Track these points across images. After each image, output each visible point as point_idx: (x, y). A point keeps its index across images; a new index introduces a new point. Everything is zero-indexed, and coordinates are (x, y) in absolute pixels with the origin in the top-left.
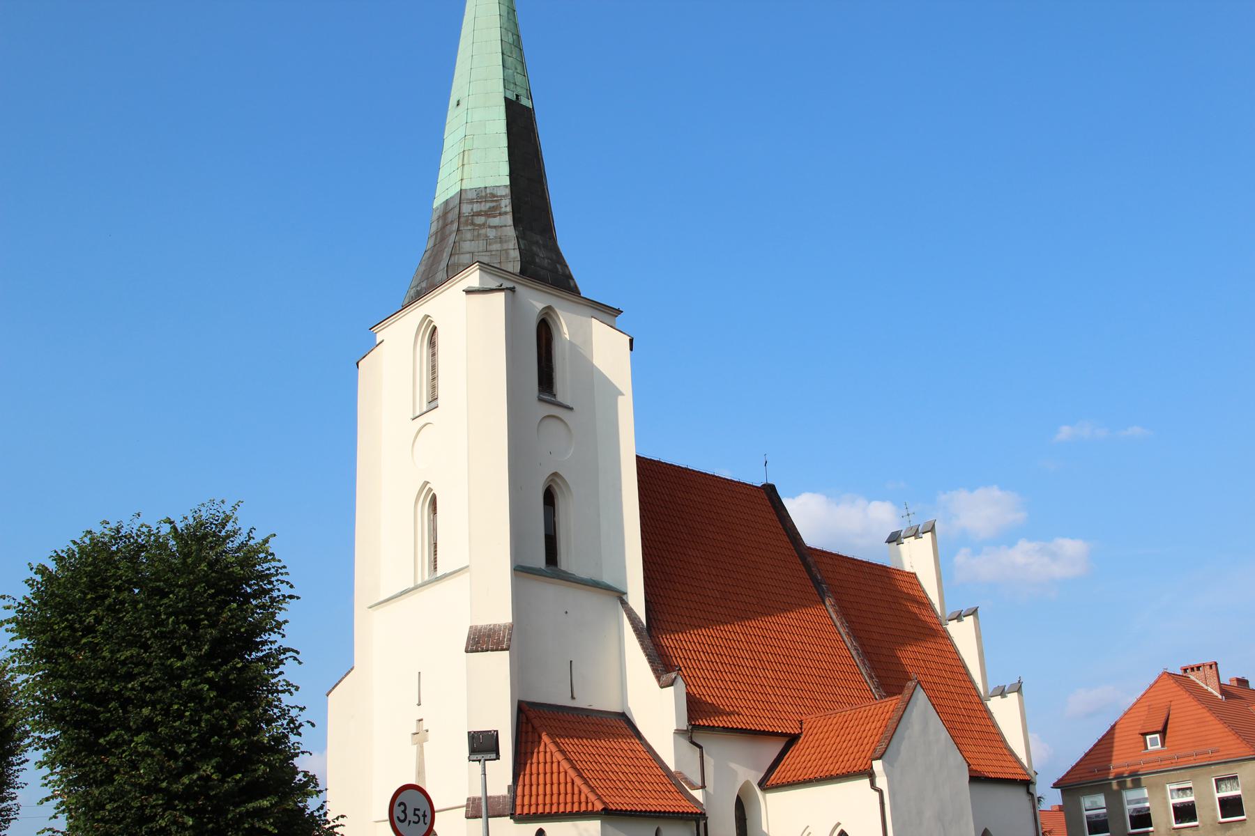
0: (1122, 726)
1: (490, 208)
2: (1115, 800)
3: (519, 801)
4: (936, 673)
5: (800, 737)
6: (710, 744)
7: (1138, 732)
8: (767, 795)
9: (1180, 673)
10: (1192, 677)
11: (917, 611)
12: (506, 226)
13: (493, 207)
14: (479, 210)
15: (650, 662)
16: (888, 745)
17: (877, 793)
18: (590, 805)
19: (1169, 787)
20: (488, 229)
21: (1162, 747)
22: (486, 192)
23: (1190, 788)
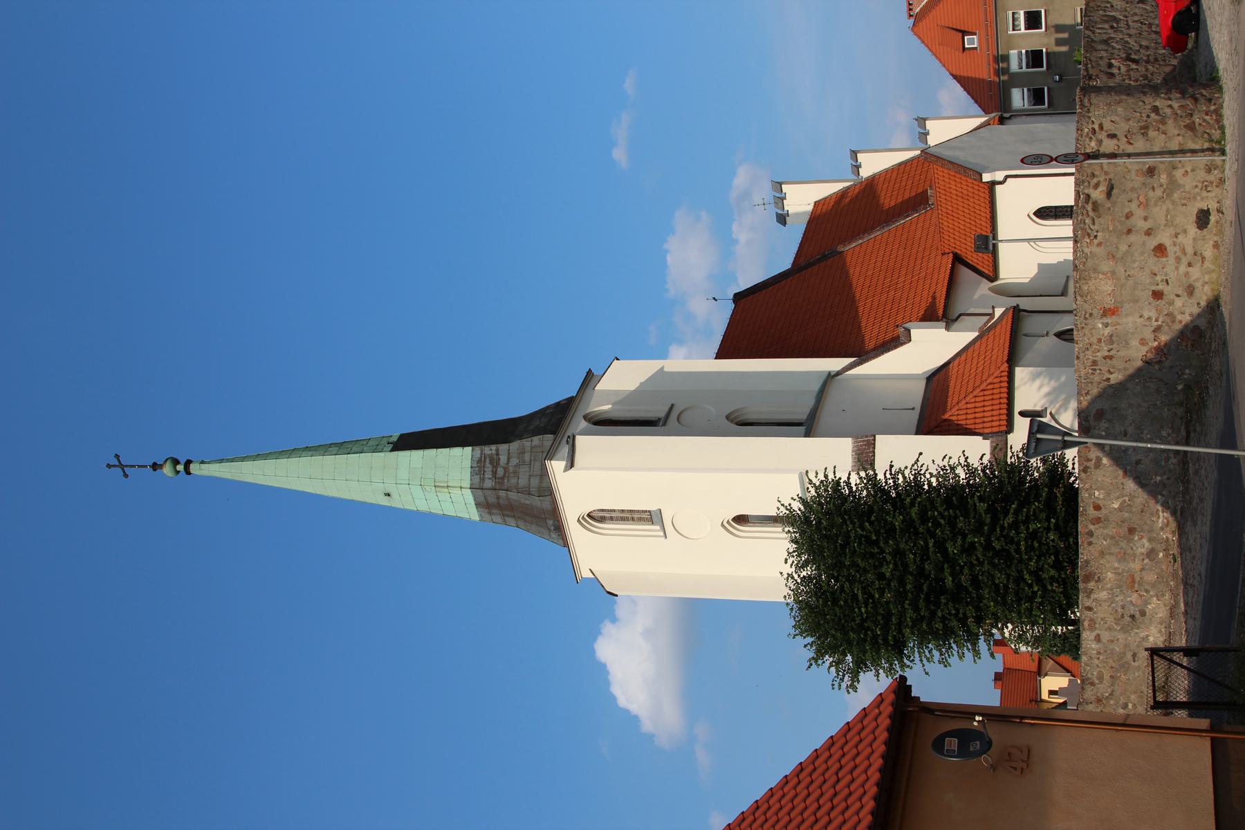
0: (954, 69)
1: (490, 463)
2: (1017, 80)
3: (995, 430)
4: (903, 184)
5: (956, 253)
6: (960, 306)
7: (960, 54)
8: (1001, 277)
9: (912, 20)
10: (918, 10)
11: (848, 200)
12: (509, 450)
13: (490, 460)
14: (491, 473)
15: (889, 351)
16: (971, 169)
17: (1008, 179)
18: (1003, 374)
19: (1011, 32)
20: (510, 464)
21: (975, 34)
22: (475, 467)
23: (1013, 13)
